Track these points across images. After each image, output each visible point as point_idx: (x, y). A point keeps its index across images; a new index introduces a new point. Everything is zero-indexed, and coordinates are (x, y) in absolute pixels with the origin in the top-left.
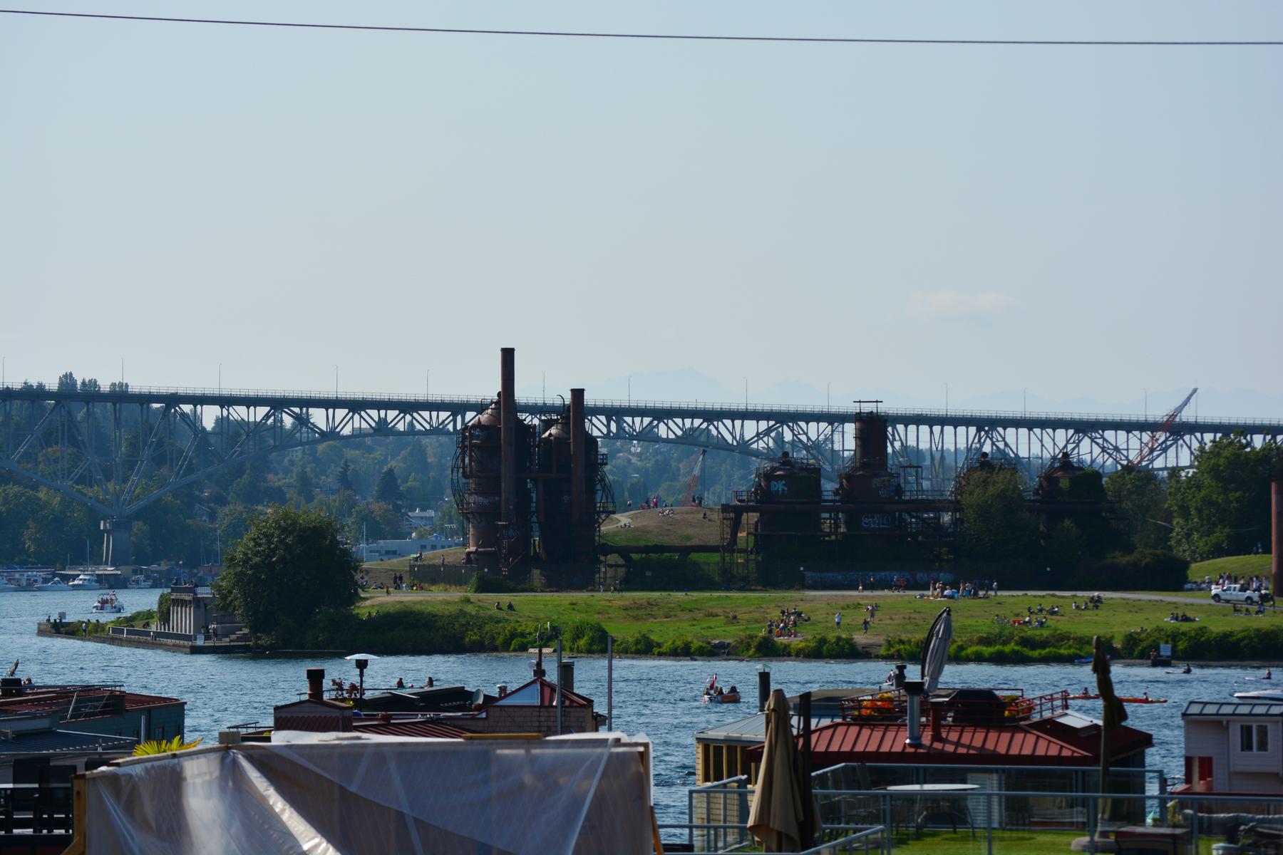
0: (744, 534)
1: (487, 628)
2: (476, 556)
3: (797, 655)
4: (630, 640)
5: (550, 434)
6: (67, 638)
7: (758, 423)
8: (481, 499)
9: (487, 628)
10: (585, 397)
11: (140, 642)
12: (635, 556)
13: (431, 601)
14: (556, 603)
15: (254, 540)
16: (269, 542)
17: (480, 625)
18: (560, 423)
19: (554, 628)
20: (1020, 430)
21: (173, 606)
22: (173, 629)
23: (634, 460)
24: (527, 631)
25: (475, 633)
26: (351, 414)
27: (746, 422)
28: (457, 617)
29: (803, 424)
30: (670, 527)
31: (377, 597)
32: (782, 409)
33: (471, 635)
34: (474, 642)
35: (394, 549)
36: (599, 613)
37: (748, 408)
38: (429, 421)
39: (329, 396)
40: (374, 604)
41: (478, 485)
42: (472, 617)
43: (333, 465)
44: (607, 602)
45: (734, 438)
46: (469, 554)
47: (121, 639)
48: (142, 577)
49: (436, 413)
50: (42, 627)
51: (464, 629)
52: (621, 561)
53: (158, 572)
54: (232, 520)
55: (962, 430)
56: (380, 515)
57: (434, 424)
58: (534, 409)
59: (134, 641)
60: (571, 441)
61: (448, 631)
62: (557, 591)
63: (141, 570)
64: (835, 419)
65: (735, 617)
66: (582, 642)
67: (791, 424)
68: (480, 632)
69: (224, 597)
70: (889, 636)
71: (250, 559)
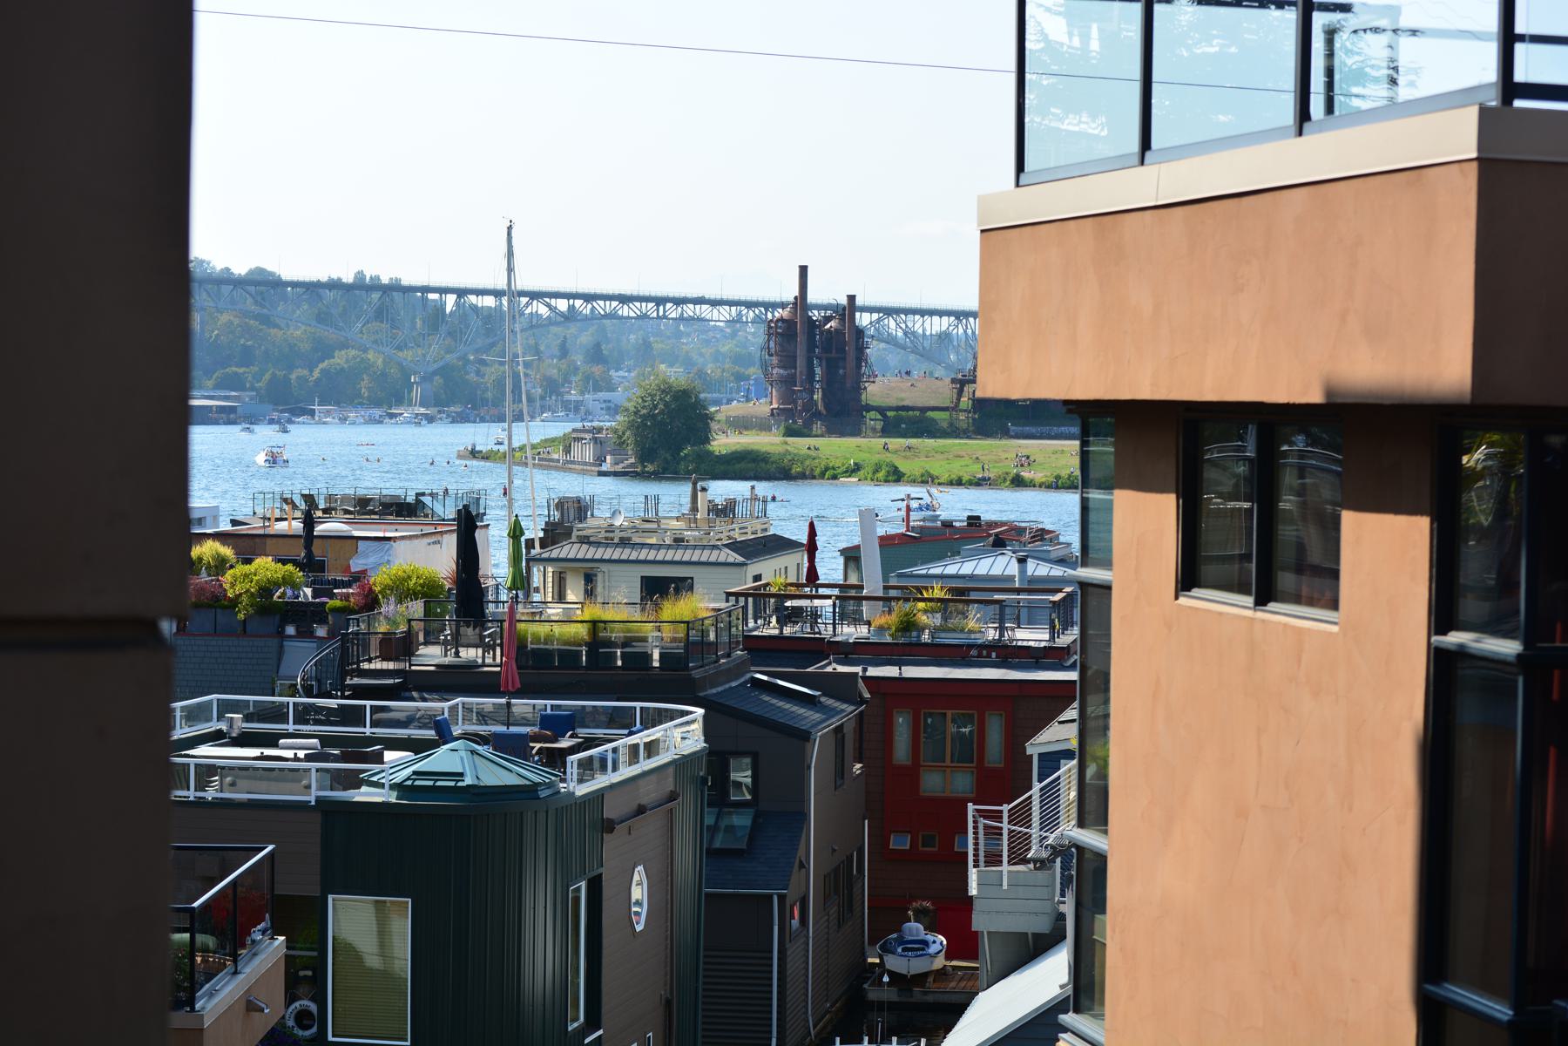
0: (966, 399)
1: (807, 463)
3: (1040, 486)
4: (917, 473)
5: (831, 327)
8: (782, 371)
9: (807, 463)
12: (890, 414)
15: (642, 398)
16: (653, 400)
19: (856, 464)
20: (934, 317)
24: (837, 465)
27: (863, 314)
28: (785, 455)
29: (903, 316)
30: (889, 392)
41: (780, 361)
42: (795, 455)
46: (772, 410)
48: (445, 416)
50: (461, 453)
52: (879, 417)
53: (456, 412)
55: (945, 319)
58: (819, 307)
63: (444, 411)
64: (443, 291)
65: (977, 458)
66: (881, 475)
69: (620, 437)
70: (344, 456)
71: (639, 411)
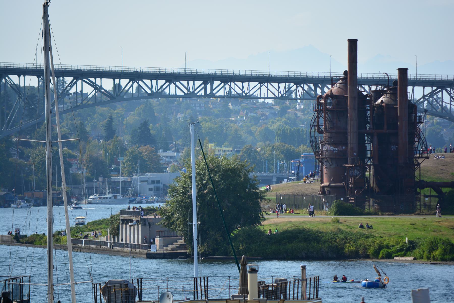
1: (360, 241)
2: (328, 189)
5: (382, 102)
6: (27, 246)
7: (424, 88)
8: (332, 148)
9: (360, 241)
10: (358, 72)
11: (99, 250)
12: (445, 190)
13: (311, 222)
14: (400, 223)
17: (355, 240)
18: (388, 93)
21: (122, 224)
22: (122, 240)
23: (299, 114)
24: (391, 244)
25: (352, 245)
26: (131, 83)
27: (416, 88)
28: (337, 234)
30: (444, 168)
31: (272, 218)
32: (369, 76)
33: (349, 247)
34: (351, 252)
35: (158, 179)
36: (434, 231)
37: (418, 77)
38: (187, 87)
39: (21, 66)
40: (271, 223)
43: (89, 118)
44: (437, 223)
45: (189, 91)
46: (323, 188)
47: (81, 248)
49: (155, 81)
51: (343, 242)
52: (434, 193)
54: (42, 158)
56: (146, 155)
57: (154, 89)
58: (370, 82)
59: (107, 251)
60: (398, 106)
61: (332, 243)
62: (393, 215)
66: (437, 253)
67: (449, 89)
68: (355, 245)
69: (169, 218)
